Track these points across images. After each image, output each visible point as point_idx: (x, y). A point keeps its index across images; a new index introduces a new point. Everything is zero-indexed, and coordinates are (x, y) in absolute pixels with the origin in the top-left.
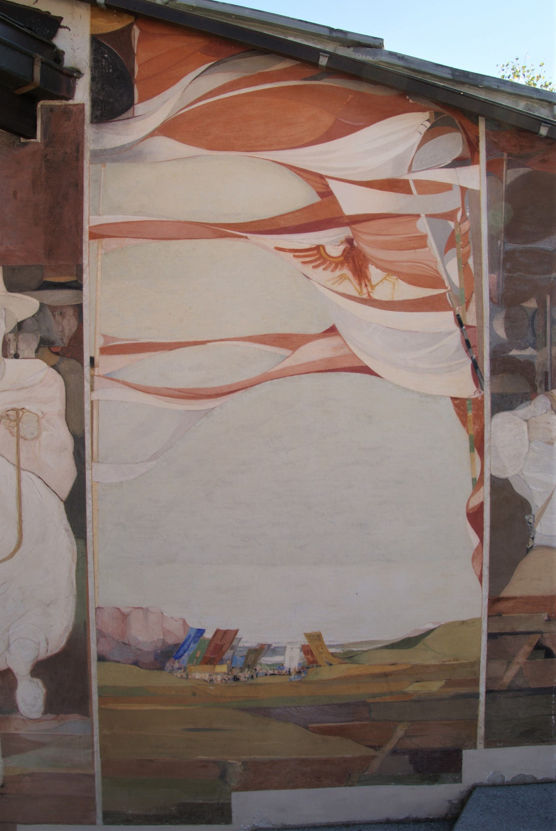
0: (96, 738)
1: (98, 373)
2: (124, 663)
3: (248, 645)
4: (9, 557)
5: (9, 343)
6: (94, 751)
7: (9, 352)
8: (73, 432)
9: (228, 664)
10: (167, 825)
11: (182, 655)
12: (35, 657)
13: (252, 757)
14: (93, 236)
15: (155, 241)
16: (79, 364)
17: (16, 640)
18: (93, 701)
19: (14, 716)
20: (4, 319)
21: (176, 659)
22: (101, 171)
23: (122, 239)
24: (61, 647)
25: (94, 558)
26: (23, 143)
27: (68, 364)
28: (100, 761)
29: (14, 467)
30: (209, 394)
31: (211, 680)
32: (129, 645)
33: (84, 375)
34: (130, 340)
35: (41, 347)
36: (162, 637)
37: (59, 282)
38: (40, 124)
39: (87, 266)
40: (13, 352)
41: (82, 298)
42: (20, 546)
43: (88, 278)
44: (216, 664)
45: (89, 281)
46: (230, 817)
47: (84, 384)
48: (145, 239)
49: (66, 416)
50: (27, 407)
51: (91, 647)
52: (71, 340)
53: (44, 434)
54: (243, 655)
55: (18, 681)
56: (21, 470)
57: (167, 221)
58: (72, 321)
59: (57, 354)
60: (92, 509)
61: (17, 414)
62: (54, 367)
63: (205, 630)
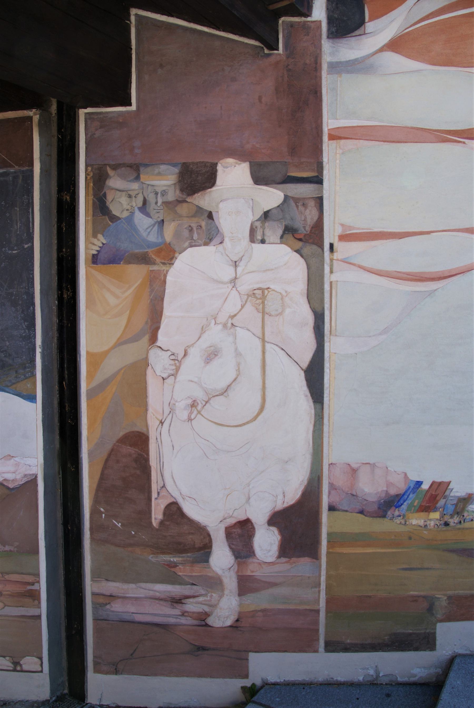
0: (323, 578)
1: (337, 257)
2: (351, 512)
3: (458, 494)
4: (253, 420)
5: (256, 229)
6: (320, 589)
7: (256, 238)
8: (314, 309)
9: (441, 511)
10: (380, 652)
11: (402, 504)
12: (272, 509)
13: (456, 592)
14: (332, 137)
15: (386, 143)
16: (320, 250)
17: (255, 494)
18: (322, 546)
19: (251, 560)
20: (251, 209)
21: (396, 508)
22: (338, 81)
23: (358, 140)
24: (296, 499)
25: (329, 420)
26: (266, 54)
27: (309, 249)
28: (325, 598)
29: (259, 340)
30: (432, 277)
31: (426, 526)
32: (356, 496)
33: (324, 259)
34: (365, 229)
35: (286, 234)
36: (385, 489)
37: (302, 177)
38: (282, 38)
39: (326, 164)
40: (259, 238)
41: (322, 192)
42: (263, 410)
43: (328, 174)
44: (431, 512)
45: (329, 176)
46: (435, 644)
47: (324, 267)
48: (377, 142)
49: (308, 294)
50: (272, 287)
51: (323, 498)
52: (312, 227)
53: (288, 311)
54: (453, 503)
55: (256, 530)
56: (266, 343)
57: (396, 126)
58: (313, 211)
59: (300, 240)
60: (330, 377)
61: (263, 293)
62: (297, 251)
63: (423, 482)
